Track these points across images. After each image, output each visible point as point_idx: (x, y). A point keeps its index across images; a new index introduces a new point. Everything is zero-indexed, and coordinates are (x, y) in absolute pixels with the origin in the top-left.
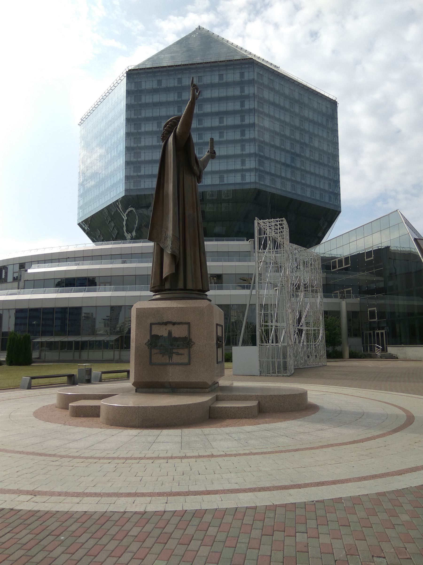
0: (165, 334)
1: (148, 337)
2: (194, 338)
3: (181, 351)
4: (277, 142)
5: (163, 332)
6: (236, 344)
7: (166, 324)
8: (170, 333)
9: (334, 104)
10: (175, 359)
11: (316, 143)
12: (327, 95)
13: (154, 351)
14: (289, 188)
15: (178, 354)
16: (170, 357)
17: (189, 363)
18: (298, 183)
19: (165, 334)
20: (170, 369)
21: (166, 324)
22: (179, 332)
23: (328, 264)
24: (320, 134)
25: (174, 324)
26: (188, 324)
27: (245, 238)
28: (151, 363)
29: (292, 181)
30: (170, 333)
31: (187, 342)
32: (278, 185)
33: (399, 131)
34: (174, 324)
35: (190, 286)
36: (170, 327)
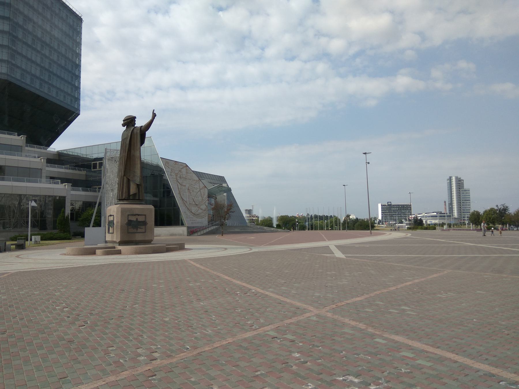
0: (135, 220)
1: (127, 221)
2: (147, 221)
3: (142, 227)
4: (63, 63)
5: (133, 218)
6: (89, 226)
7: (135, 215)
8: (137, 219)
9: (79, 20)
10: (139, 230)
11: (30, 27)
12: (68, 4)
13: (129, 227)
14: (18, 76)
15: (140, 228)
16: (137, 230)
17: (145, 232)
18: (46, 82)
19: (135, 220)
20: (137, 234)
21: (135, 215)
22: (141, 219)
23: (60, 159)
24: (35, 20)
25: (139, 215)
26: (145, 215)
27: (16, 134)
28: (128, 233)
29: (41, 80)
30: (137, 219)
31: (144, 223)
32: (37, 85)
33: (98, 42)
34: (139, 215)
35: (141, 198)
36: (137, 217)
